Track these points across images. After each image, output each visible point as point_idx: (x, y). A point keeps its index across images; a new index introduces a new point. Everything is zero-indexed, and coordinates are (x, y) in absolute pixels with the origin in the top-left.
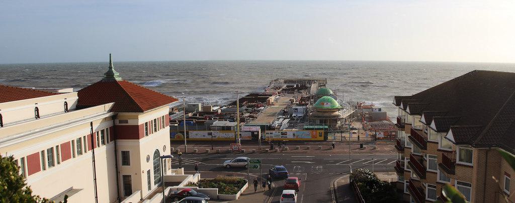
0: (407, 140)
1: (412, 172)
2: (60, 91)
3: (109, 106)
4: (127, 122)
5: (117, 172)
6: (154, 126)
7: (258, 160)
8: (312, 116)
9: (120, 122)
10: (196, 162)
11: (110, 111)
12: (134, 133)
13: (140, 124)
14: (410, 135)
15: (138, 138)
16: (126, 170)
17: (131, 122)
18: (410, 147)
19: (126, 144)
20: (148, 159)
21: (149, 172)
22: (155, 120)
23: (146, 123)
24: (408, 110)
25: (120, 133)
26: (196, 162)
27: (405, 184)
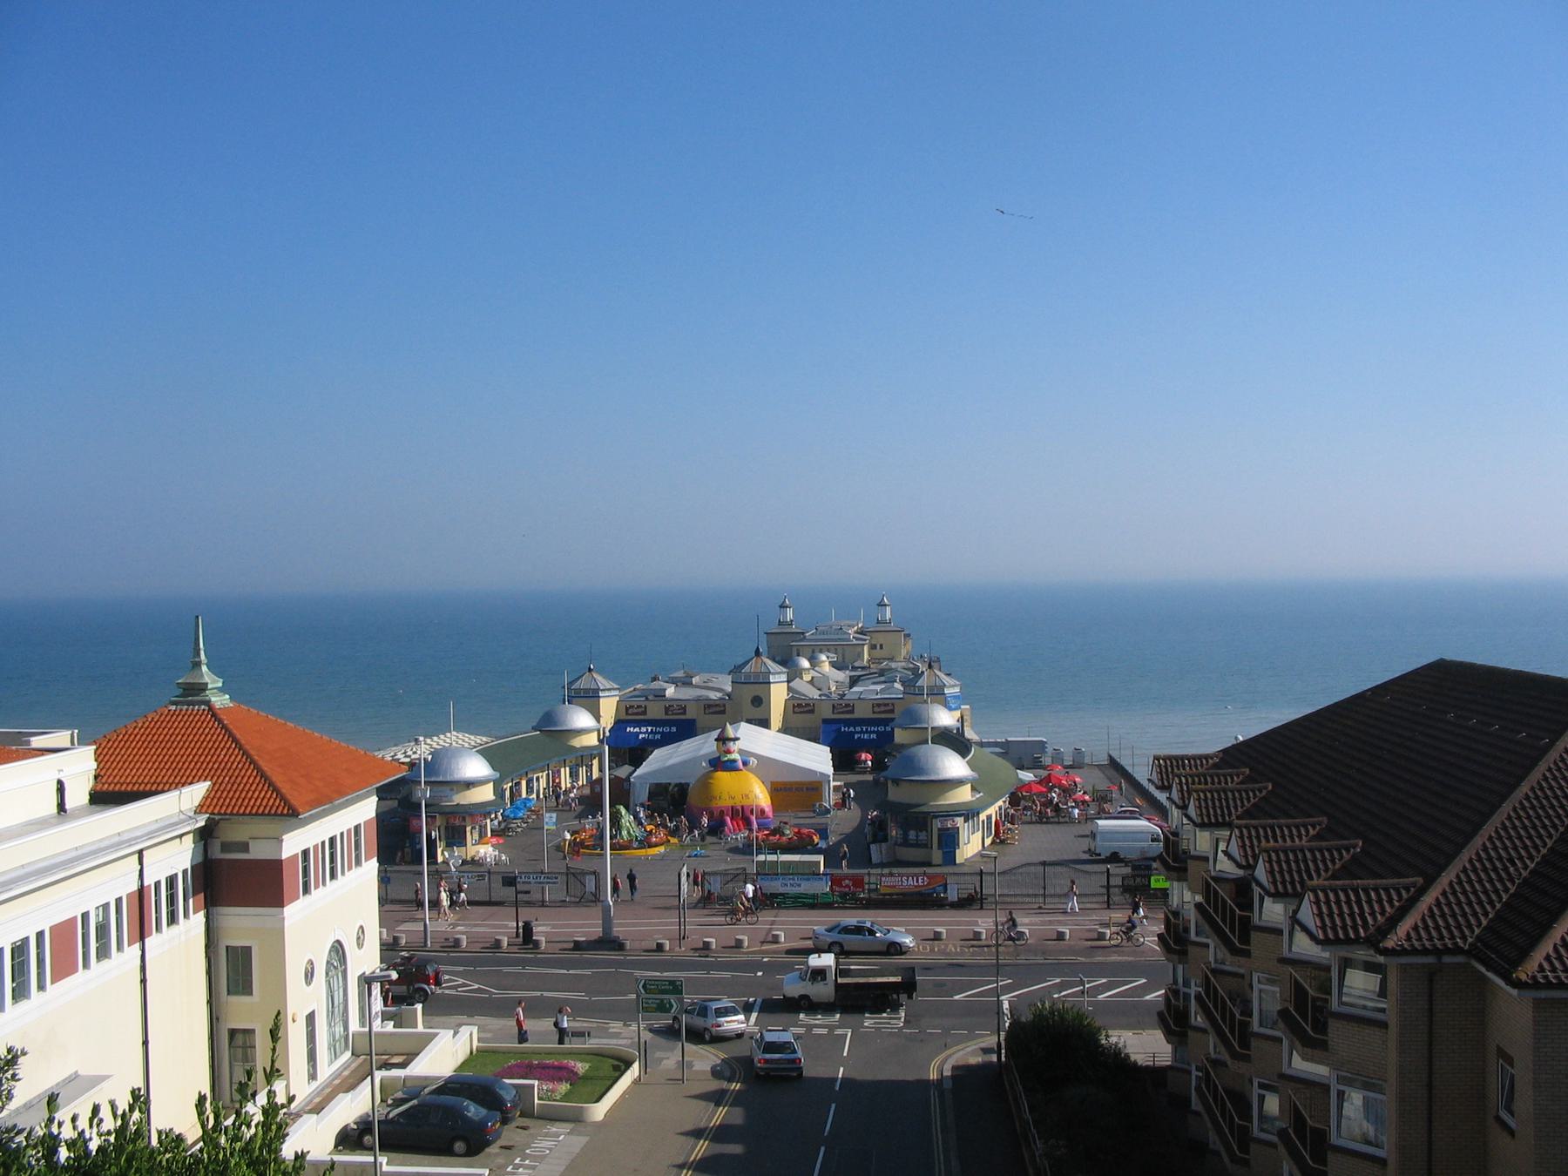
0: (1192, 915)
1: (1212, 946)
2: (37, 742)
3: (197, 792)
4: (244, 847)
5: (214, 1019)
6: (331, 859)
7: (672, 983)
8: (1269, 780)
9: (226, 847)
10: (461, 981)
11: (199, 810)
12: (265, 885)
13: (284, 856)
14: (1199, 898)
15: (282, 905)
16: (244, 1012)
17: (259, 851)
18: (1205, 940)
19: (241, 923)
20: (309, 976)
21: (311, 1018)
22: (332, 840)
23: (305, 853)
24: (1192, 811)
25: (232, 878)
26: (461, 981)
27: (1195, 1073)
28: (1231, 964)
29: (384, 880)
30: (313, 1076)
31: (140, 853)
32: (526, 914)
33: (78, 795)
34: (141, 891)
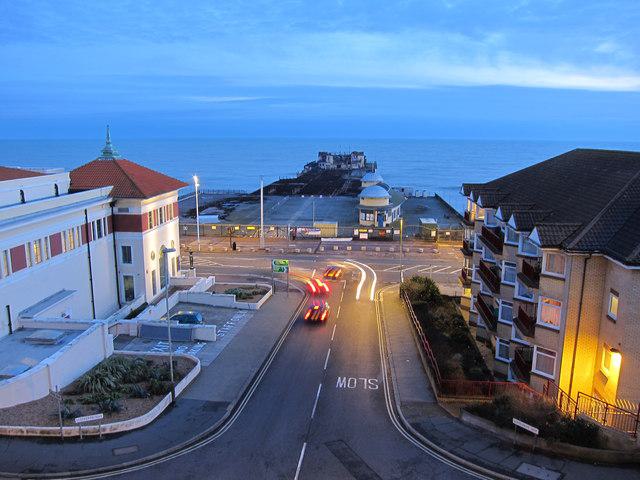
4: (127, 210)
6: (160, 216)
11: (109, 196)
12: (136, 224)
17: (133, 212)
18: (512, 284)
19: (126, 238)
21: (153, 273)
25: (124, 223)
28: (525, 341)
29: (181, 227)
30: (154, 293)
31: (57, 195)
32: (233, 240)
33: (64, 188)
34: (87, 225)
